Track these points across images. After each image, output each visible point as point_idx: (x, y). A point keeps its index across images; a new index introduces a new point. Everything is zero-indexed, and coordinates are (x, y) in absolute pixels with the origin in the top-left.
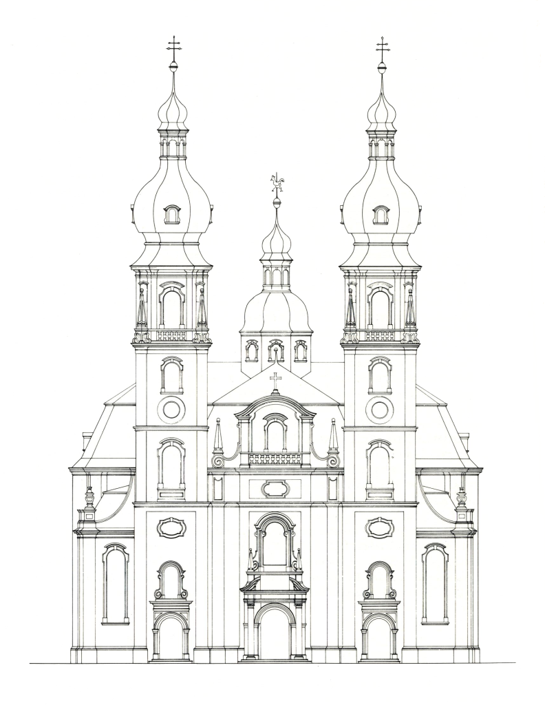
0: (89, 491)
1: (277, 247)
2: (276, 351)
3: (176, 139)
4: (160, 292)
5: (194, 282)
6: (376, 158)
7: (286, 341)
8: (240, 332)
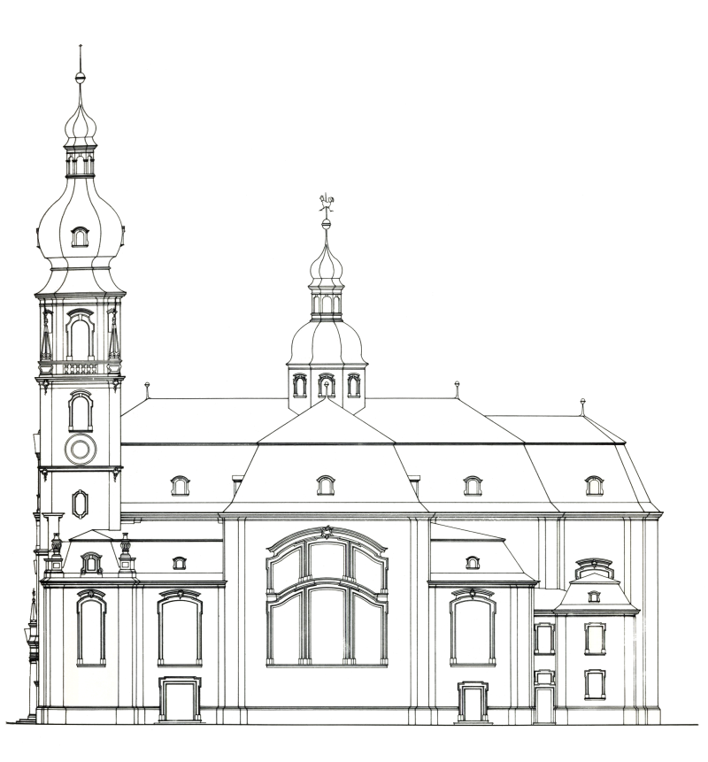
0: (57, 538)
1: (327, 271)
2: (327, 385)
3: (84, 155)
4: (66, 322)
5: (106, 310)
6: (75, 176)
7: (337, 374)
8: (287, 364)
